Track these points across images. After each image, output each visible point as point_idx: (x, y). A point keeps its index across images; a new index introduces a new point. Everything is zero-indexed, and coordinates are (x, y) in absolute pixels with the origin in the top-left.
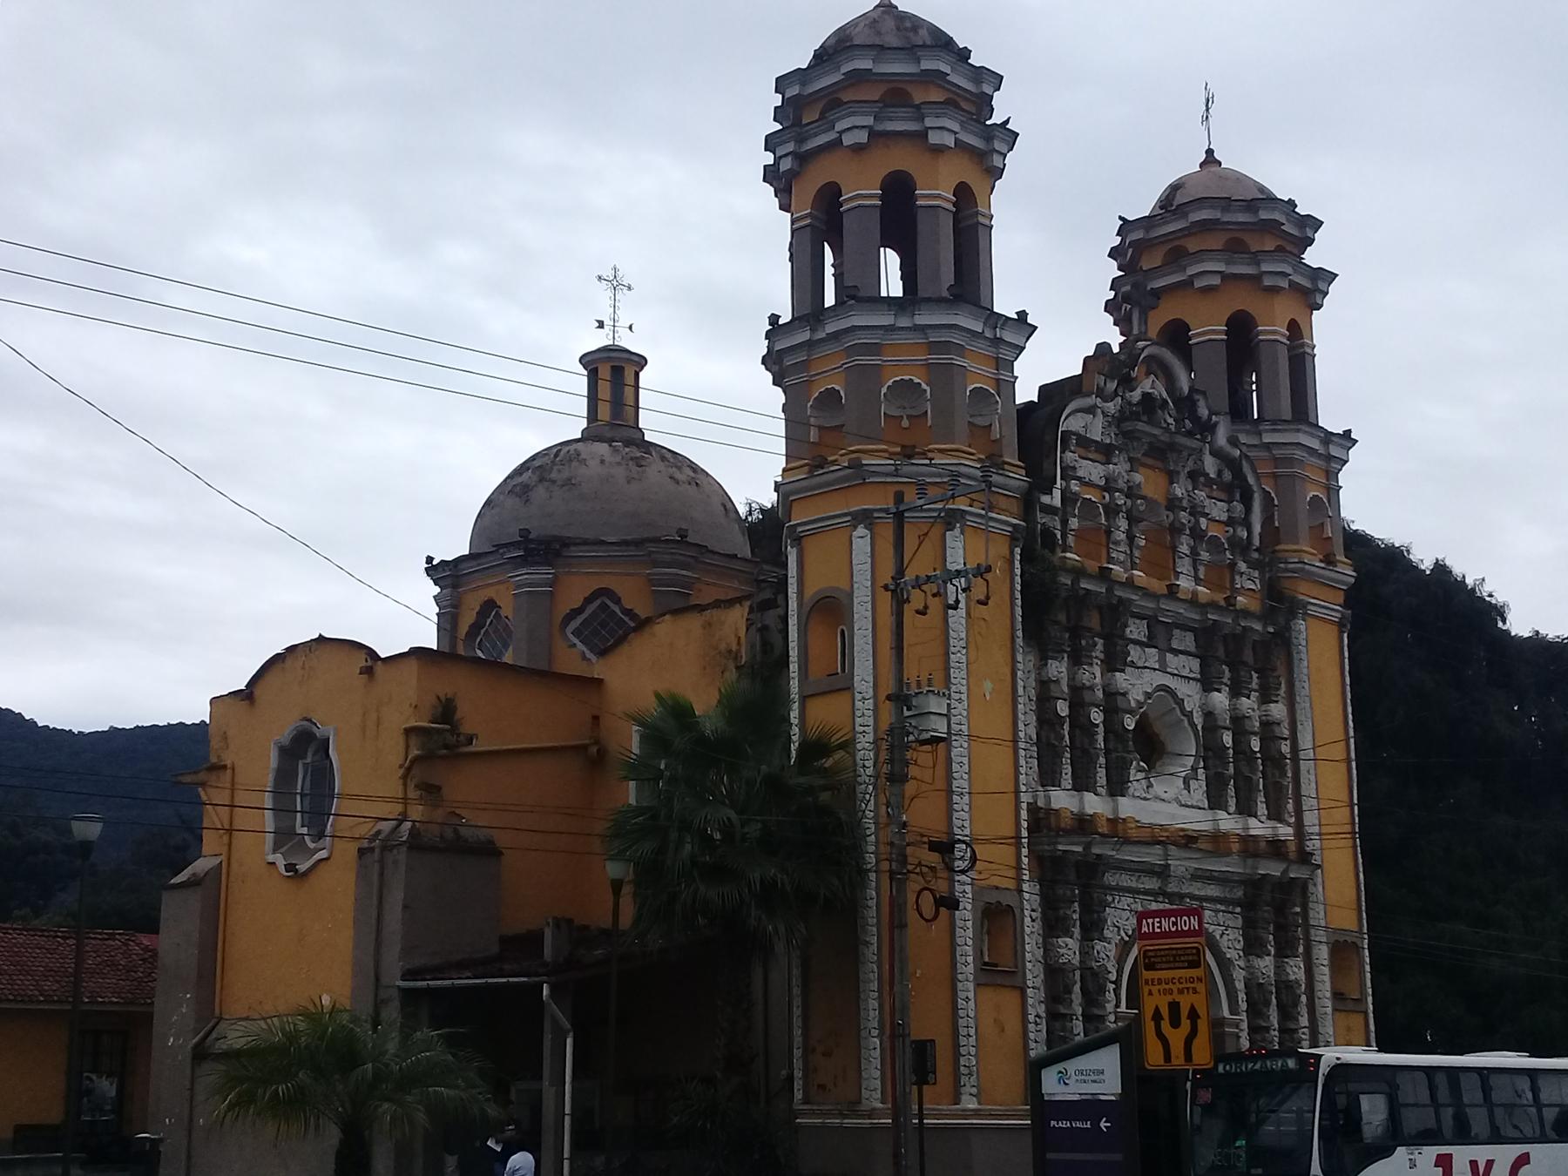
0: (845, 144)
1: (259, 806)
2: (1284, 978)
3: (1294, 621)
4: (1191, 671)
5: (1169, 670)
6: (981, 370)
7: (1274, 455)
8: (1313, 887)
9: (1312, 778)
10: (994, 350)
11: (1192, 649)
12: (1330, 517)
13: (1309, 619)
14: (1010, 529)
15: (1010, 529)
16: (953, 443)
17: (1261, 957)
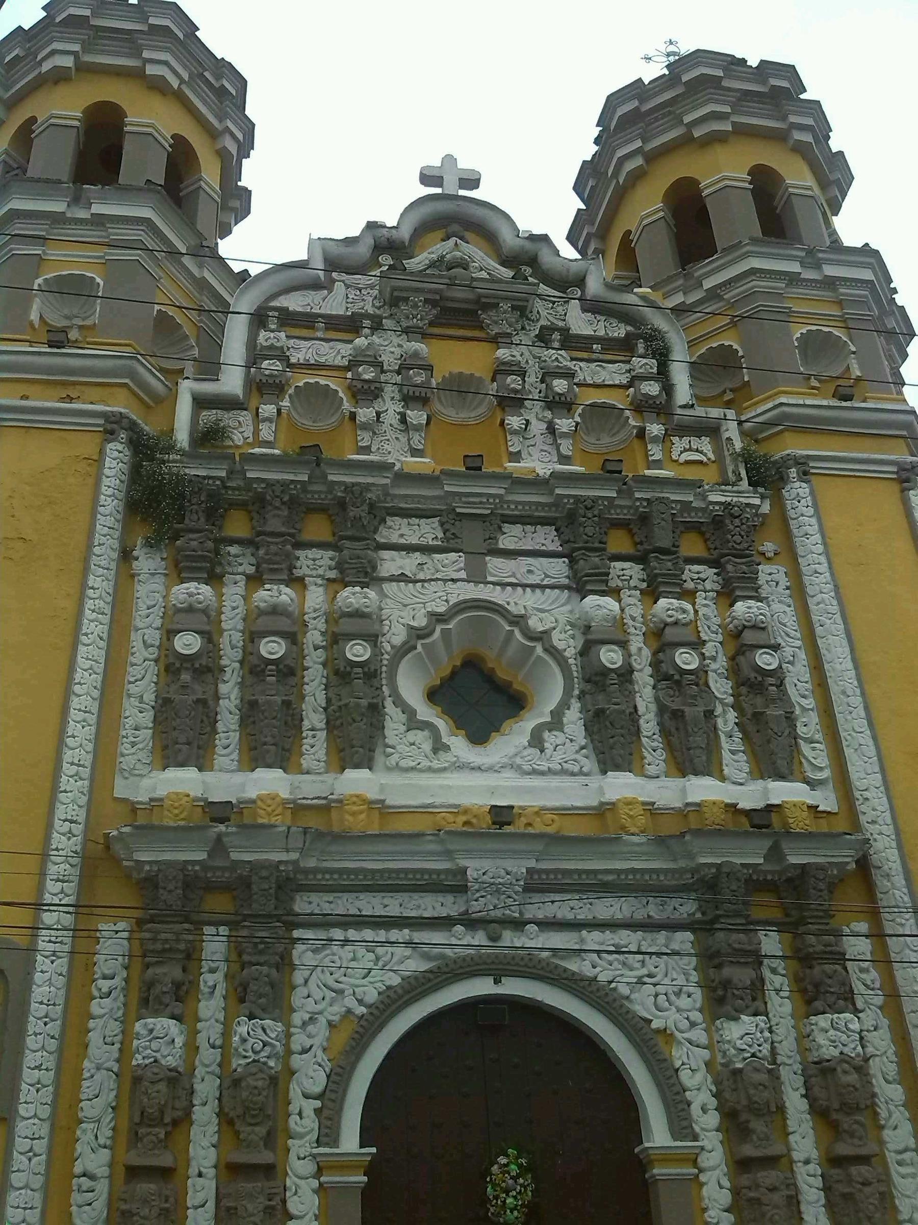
0: (120, 182)
1: (87, 904)
2: (813, 1056)
3: (788, 487)
4: (547, 576)
5: (490, 579)
6: (73, 256)
7: (728, 301)
8: (885, 882)
9: (857, 701)
10: (104, 234)
11: (555, 546)
12: (854, 353)
13: (813, 478)
14: (101, 421)
15: (101, 421)
16: (422, 457)
17: (736, 1019)
